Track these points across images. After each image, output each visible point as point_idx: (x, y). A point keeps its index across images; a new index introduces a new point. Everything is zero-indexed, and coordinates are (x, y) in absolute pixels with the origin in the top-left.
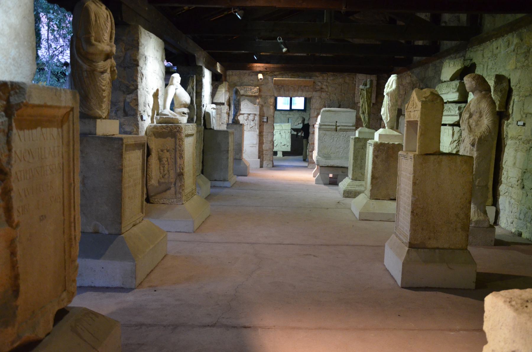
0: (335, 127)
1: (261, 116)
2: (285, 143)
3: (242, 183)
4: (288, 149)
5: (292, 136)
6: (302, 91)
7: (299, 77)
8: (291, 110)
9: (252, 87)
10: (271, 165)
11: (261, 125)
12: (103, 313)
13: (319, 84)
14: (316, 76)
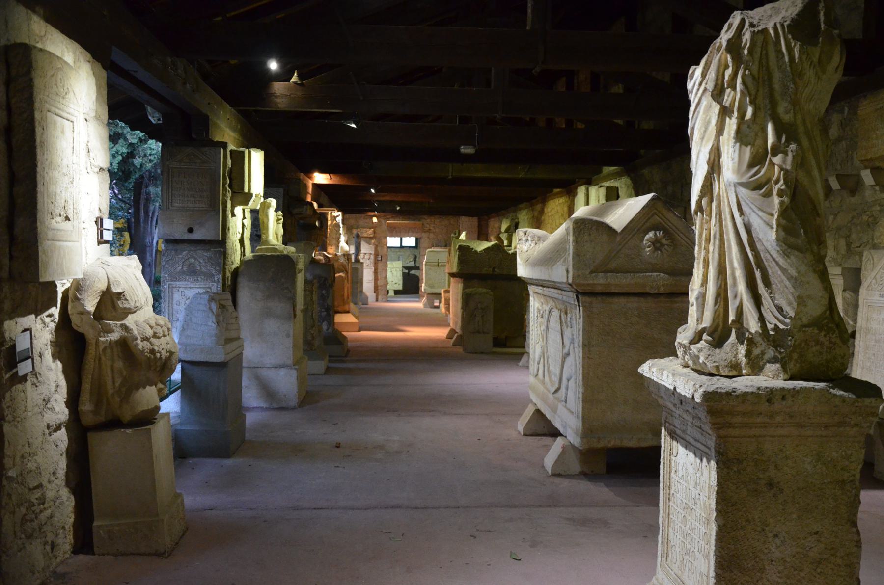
0: (437, 264)
1: (376, 255)
2: (397, 281)
3: (366, 308)
4: (400, 287)
5: (404, 275)
6: (413, 232)
7: (409, 219)
8: (402, 247)
9: (368, 229)
10: (385, 300)
11: (376, 262)
12: (209, 461)
13: (428, 226)
14: (425, 219)
